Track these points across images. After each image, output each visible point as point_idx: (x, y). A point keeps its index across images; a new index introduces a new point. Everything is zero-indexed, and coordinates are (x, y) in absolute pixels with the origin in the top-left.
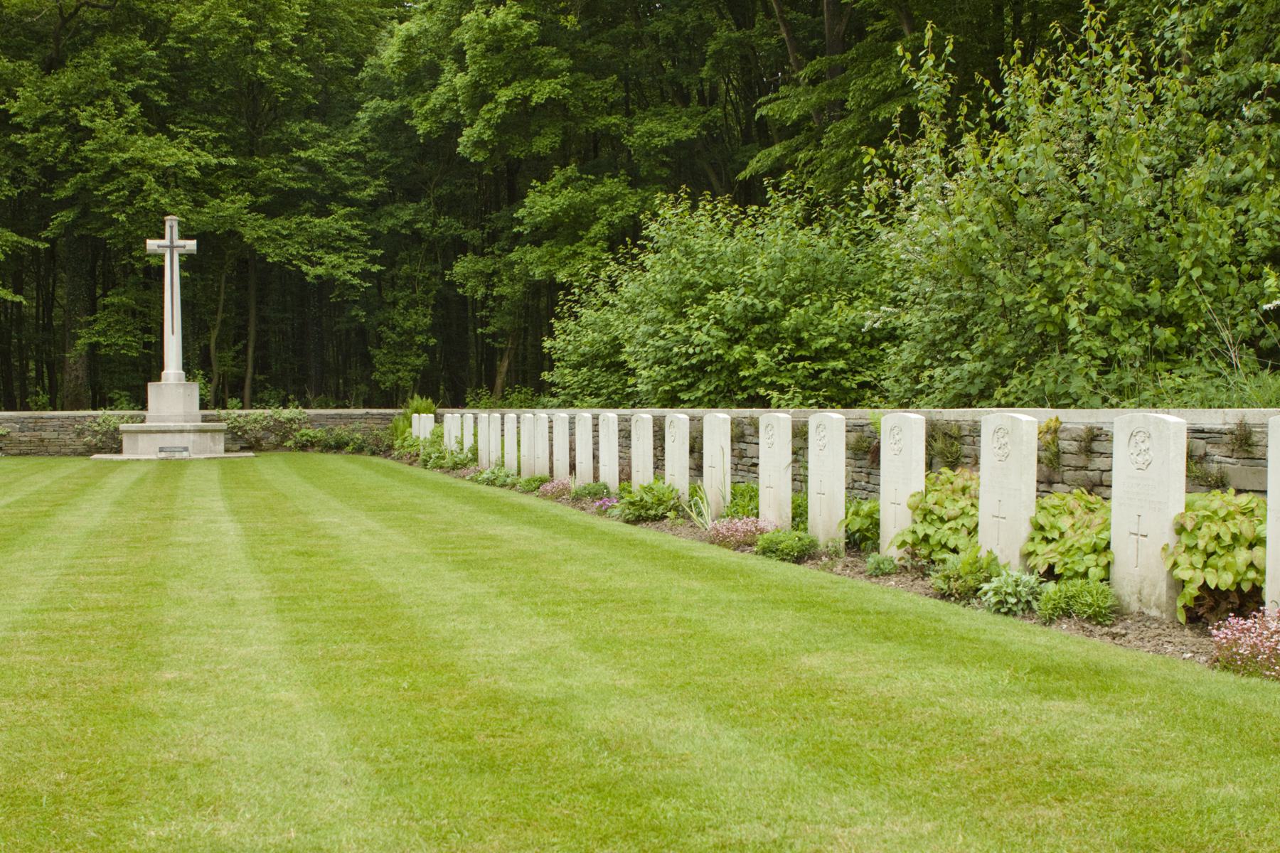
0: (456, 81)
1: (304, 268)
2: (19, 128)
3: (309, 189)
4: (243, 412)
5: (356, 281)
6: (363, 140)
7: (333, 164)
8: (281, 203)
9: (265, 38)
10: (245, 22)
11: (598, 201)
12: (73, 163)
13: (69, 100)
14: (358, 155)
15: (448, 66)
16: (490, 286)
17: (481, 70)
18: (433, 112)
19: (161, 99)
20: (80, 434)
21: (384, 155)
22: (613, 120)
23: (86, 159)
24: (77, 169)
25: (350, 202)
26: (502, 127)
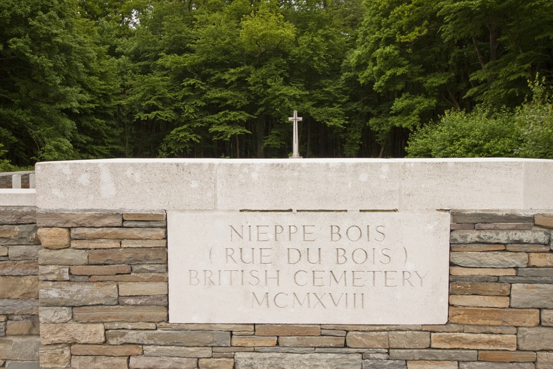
1: (327, 123)
2: (250, 85)
5: (342, 127)
8: (319, 104)
10: (311, 52)
13: (264, 77)
15: (370, 63)
18: (366, 77)
19: (287, 75)
21: (348, 88)
22: (421, 78)
23: (267, 93)
24: (265, 96)
25: (339, 103)
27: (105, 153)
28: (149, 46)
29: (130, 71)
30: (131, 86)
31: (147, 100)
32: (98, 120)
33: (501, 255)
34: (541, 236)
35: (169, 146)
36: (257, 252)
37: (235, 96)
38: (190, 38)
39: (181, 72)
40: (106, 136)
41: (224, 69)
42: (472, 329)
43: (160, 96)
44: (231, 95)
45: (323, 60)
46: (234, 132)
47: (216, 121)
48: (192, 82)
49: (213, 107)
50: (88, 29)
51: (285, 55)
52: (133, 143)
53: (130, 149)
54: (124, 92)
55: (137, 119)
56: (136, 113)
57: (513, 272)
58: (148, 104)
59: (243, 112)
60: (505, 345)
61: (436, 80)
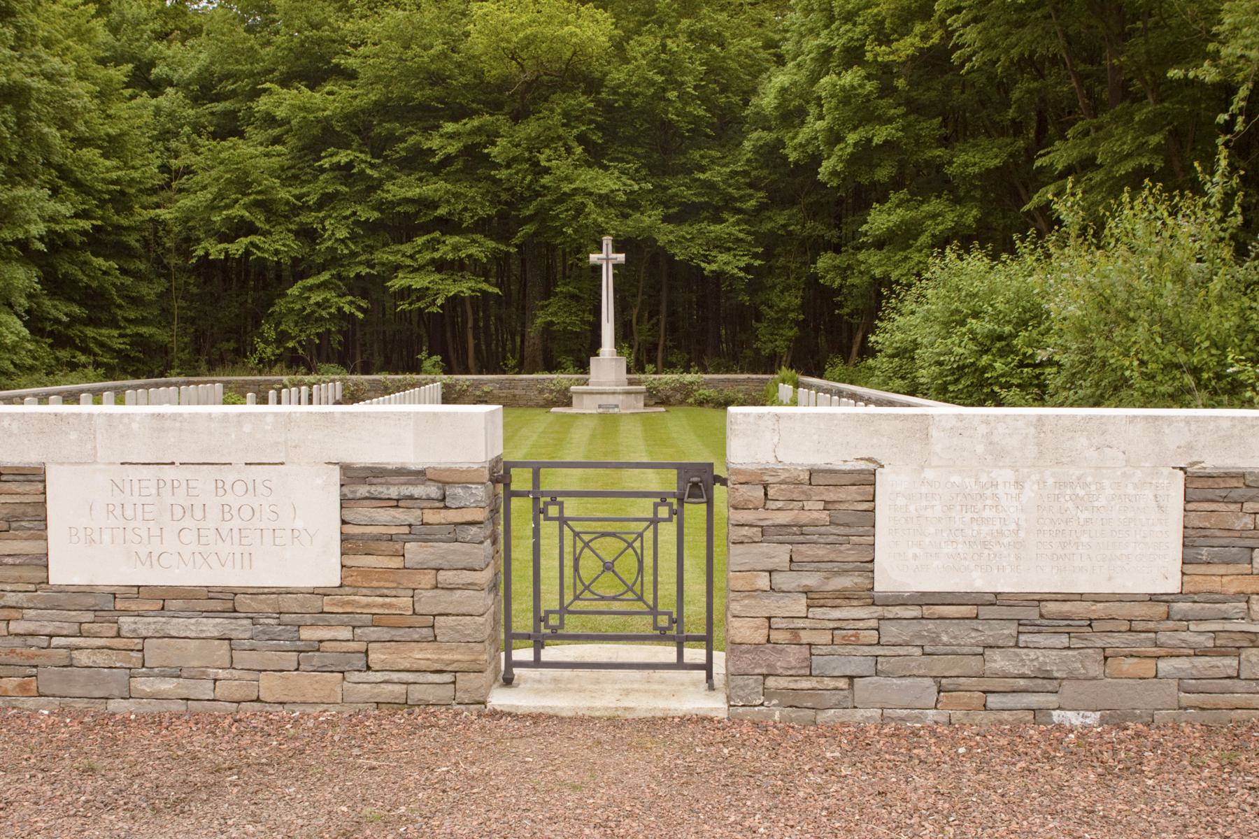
0: (815, 126)
1: (703, 265)
2: (496, 166)
3: (706, 202)
4: (657, 376)
5: (742, 274)
6: (748, 161)
7: (724, 182)
8: (684, 214)
9: (674, 89)
10: (659, 79)
11: (925, 217)
12: (534, 190)
13: (535, 145)
14: (745, 174)
16: (845, 278)
17: (834, 119)
19: (597, 138)
20: (541, 391)
21: (765, 172)
22: (938, 152)
23: (543, 187)
24: (538, 194)
25: (739, 211)
26: (852, 160)
27: (117, 346)
28: (237, 61)
29: (187, 129)
30: (188, 170)
31: (227, 207)
32: (99, 262)
33: (392, 512)
34: (433, 491)
35: (282, 327)
36: (139, 508)
37: (457, 196)
38: (343, 41)
39: (316, 131)
40: (119, 301)
41: (431, 122)
42: (365, 591)
43: (259, 197)
44: (447, 192)
45: (693, 98)
46: (453, 290)
47: (408, 262)
48: (343, 157)
49: (400, 224)
50: (78, 26)
51: (593, 85)
52: (193, 321)
53: (186, 334)
54: (168, 186)
55: (200, 257)
56: (198, 241)
57: (406, 530)
58: (228, 218)
59: (478, 237)
60: (400, 609)
61: (974, 159)
